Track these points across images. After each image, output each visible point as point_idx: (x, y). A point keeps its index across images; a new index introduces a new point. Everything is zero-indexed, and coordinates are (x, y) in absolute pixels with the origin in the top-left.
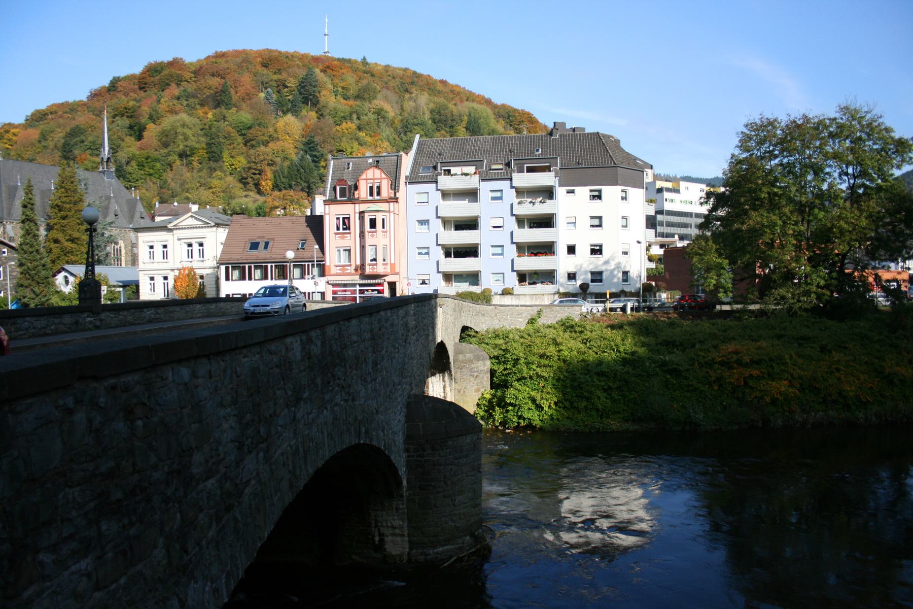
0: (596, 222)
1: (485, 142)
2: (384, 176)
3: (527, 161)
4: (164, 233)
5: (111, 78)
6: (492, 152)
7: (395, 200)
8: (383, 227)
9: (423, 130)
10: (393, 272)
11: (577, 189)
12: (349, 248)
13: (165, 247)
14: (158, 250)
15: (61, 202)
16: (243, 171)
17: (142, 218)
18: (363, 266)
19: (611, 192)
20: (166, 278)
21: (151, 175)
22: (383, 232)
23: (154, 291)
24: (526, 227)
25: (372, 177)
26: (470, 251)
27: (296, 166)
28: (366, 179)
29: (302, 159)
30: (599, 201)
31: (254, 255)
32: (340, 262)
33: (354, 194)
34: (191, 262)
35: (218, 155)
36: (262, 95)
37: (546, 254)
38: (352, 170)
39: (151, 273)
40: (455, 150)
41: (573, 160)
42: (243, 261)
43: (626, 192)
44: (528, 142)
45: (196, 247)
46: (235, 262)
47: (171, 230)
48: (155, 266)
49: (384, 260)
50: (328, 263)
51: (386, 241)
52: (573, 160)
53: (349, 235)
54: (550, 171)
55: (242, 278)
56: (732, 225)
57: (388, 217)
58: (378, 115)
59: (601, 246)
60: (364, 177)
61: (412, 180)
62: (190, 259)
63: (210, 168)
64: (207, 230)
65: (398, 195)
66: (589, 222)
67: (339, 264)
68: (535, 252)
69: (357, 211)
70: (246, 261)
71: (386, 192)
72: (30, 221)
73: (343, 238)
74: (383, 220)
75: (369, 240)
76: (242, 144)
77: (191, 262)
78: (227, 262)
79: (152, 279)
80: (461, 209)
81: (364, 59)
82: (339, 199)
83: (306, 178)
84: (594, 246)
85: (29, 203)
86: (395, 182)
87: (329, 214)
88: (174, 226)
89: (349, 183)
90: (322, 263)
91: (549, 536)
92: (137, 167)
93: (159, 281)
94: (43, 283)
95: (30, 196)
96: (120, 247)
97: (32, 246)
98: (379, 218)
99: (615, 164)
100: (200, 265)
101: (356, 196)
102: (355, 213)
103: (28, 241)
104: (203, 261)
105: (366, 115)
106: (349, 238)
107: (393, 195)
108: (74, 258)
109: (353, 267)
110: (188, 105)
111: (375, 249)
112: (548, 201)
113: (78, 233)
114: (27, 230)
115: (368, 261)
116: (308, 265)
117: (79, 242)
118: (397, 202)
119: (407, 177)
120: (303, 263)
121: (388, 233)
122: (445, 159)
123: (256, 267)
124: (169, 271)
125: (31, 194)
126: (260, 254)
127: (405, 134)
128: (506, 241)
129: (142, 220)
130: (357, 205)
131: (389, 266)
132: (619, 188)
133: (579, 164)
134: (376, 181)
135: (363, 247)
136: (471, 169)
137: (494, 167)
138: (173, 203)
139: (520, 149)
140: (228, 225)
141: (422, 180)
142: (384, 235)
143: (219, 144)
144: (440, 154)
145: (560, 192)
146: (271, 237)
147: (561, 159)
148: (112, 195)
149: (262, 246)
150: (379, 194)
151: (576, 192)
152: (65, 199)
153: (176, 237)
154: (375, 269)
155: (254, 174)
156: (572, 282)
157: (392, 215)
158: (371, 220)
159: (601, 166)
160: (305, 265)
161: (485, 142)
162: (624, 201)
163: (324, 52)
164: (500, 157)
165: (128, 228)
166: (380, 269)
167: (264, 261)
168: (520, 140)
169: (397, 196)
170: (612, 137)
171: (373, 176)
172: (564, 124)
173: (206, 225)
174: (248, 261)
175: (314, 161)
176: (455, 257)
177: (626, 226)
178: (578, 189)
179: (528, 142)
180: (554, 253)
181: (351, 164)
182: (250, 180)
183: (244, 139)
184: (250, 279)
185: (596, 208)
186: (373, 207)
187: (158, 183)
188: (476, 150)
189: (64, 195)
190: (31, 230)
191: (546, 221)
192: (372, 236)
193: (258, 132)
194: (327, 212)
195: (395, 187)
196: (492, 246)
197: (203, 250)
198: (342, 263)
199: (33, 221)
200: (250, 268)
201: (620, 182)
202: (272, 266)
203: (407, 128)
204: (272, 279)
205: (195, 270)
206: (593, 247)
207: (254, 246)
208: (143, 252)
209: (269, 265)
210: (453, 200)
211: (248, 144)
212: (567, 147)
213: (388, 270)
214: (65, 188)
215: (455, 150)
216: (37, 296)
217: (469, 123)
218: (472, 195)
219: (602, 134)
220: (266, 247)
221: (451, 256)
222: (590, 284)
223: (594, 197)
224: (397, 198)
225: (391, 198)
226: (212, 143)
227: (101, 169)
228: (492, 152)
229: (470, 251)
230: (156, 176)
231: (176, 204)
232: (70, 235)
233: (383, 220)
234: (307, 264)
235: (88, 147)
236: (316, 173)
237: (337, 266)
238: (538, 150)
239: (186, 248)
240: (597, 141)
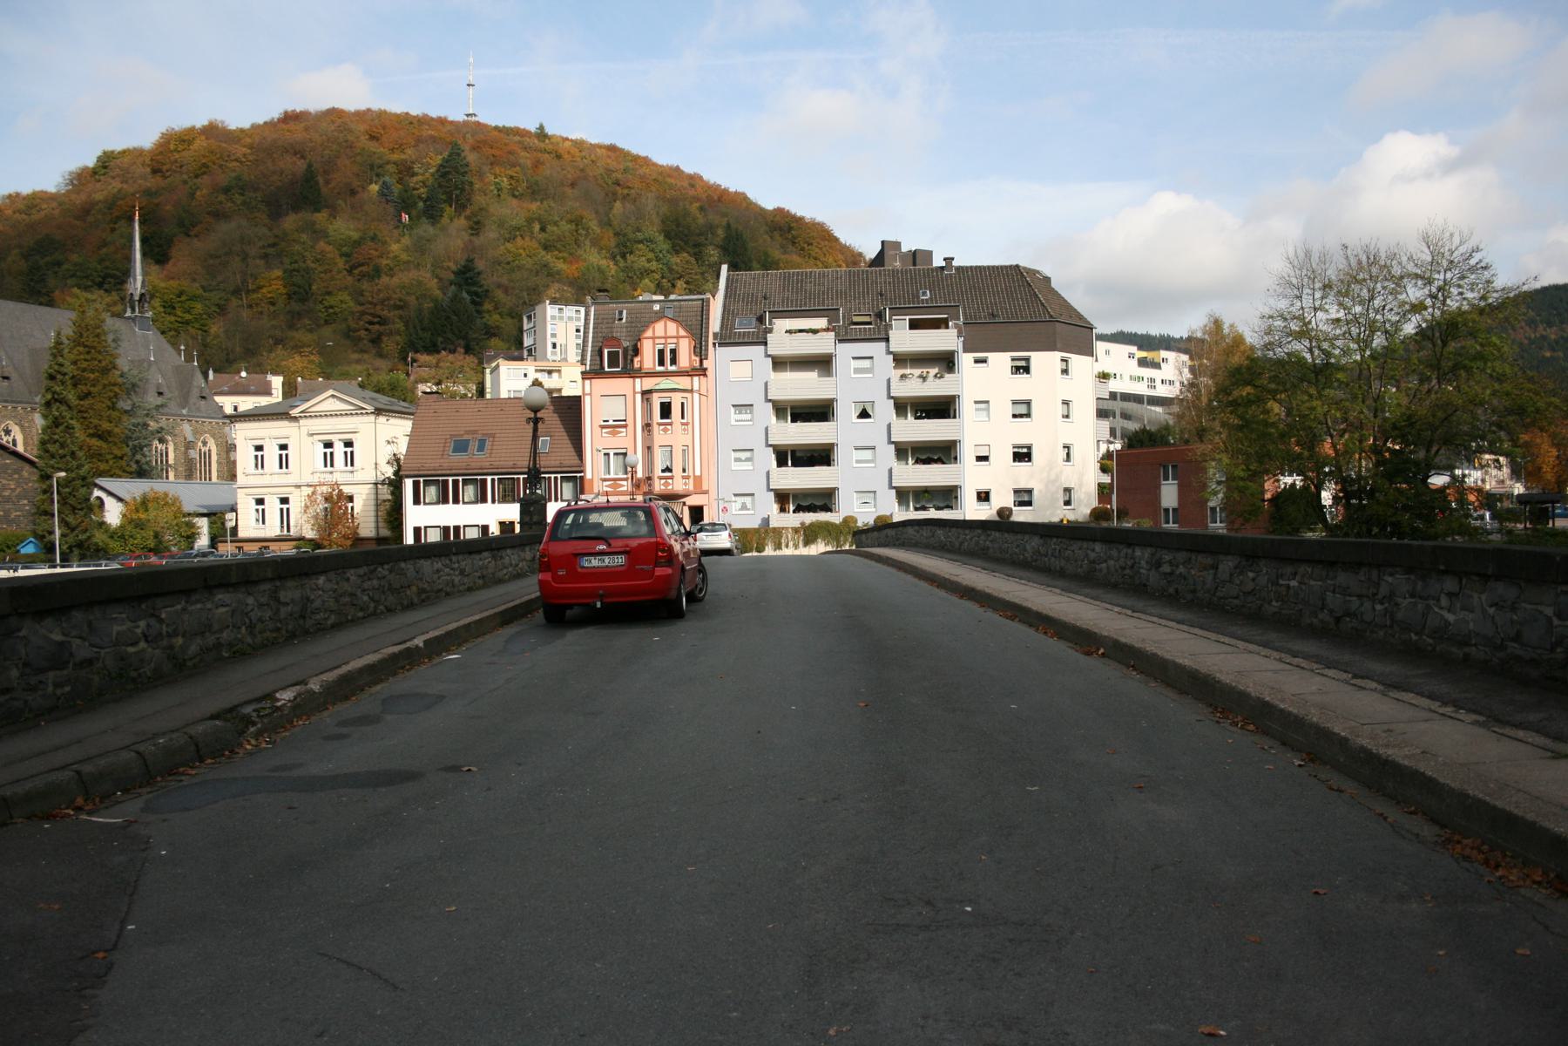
0: (1022, 409)
1: (837, 278)
2: (682, 332)
3: (907, 310)
4: (285, 423)
5: (99, 153)
6: (850, 296)
7: (702, 372)
8: (683, 417)
9: (652, 251)
10: (698, 491)
11: (992, 356)
12: (624, 451)
13: (283, 447)
14: (271, 454)
15: (78, 369)
16: (350, 318)
17: (203, 397)
19: (1045, 362)
20: (284, 501)
21: (187, 323)
22: (683, 424)
23: (264, 523)
24: (909, 415)
26: (820, 456)
27: (444, 311)
28: (654, 338)
29: (455, 298)
30: (1025, 375)
31: (459, 460)
32: (609, 473)
33: (632, 361)
34: (331, 473)
35: (305, 290)
36: (375, 188)
37: (940, 461)
38: (627, 322)
39: (259, 493)
40: (788, 290)
41: (983, 310)
42: (444, 472)
43: (1066, 361)
44: (907, 279)
45: (339, 449)
46: (430, 472)
47: (295, 419)
48: (266, 480)
49: (684, 471)
50: (589, 475)
51: (687, 440)
52: (983, 310)
53: (624, 430)
54: (947, 327)
57: (690, 400)
58: (577, 225)
59: (1029, 448)
60: (649, 333)
61: (728, 339)
62: (349, 468)
63: (289, 312)
64: (360, 418)
65: (706, 363)
66: (1010, 410)
67: (608, 476)
68: (924, 457)
69: (638, 389)
70: (448, 472)
71: (686, 359)
72: (60, 402)
73: (614, 434)
74: (683, 404)
75: (659, 437)
76: (345, 273)
77: (331, 473)
78: (416, 473)
79: (260, 502)
80: (804, 386)
81: (541, 128)
82: (606, 369)
83: (460, 332)
84: (282, 527)
85: (59, 372)
86: (701, 348)
87: (590, 394)
88: (302, 412)
89: (626, 344)
90: (578, 475)
91: (1414, 637)
92: (162, 310)
93: (273, 507)
94: (81, 509)
95: (60, 360)
96: (210, 450)
97: (63, 446)
98: (676, 400)
99: (1051, 316)
100: (348, 478)
101: (637, 365)
102: (635, 393)
103: (56, 437)
104: (352, 472)
105: (556, 224)
106: (624, 434)
107: (697, 364)
108: (103, 466)
110: (244, 203)
111: (668, 454)
112: (947, 375)
113: (108, 424)
114: (56, 418)
115: (658, 472)
116: (556, 478)
117: (110, 439)
118: (705, 375)
119: (715, 335)
120: (516, 476)
121: (690, 426)
122: (774, 304)
123: (465, 482)
124: (293, 489)
125: (62, 356)
126: (474, 459)
127: (624, 256)
128: (880, 440)
129: (203, 402)
130: (638, 381)
131: (691, 480)
132: (1058, 355)
133: (993, 316)
134: (669, 341)
135: (649, 449)
136: (821, 323)
137: (856, 319)
138: (239, 372)
139: (895, 291)
140: (412, 414)
141: (741, 341)
142: (685, 430)
143: (307, 270)
144: (765, 298)
145: (966, 360)
146: (490, 432)
147: (964, 308)
148: (152, 359)
149: (474, 446)
150: (674, 361)
151: (989, 360)
152: (85, 365)
153: (304, 431)
154: (669, 484)
155: (371, 323)
156: (984, 506)
157: (696, 396)
158: (662, 404)
159: (1029, 319)
160: (550, 478)
161: (837, 278)
162: (1065, 376)
163: (467, 115)
164: (864, 304)
165: (179, 416)
166: (678, 485)
167: (480, 471)
168: (893, 276)
169: (705, 366)
170: (1038, 272)
171: (664, 333)
172: (897, 245)
173: (359, 412)
174: (454, 472)
175: (473, 302)
176: (794, 465)
177: (1067, 417)
178: (992, 357)
179: (907, 279)
180: (956, 458)
181: (625, 312)
182: (363, 333)
183: (347, 262)
184: (456, 501)
185: (1022, 387)
187: (200, 338)
188: (823, 292)
189: (82, 357)
190: (63, 418)
191: (942, 408)
192: (665, 430)
193: (372, 252)
194: (587, 390)
195: (700, 351)
196: (857, 448)
197: (262, 456)
198: (612, 476)
199: (66, 403)
200: (456, 483)
201: (1059, 345)
202: (493, 480)
203: (626, 247)
204: (493, 501)
205: (341, 487)
206: (1016, 450)
207: (461, 446)
208: (244, 458)
209: (489, 478)
210: (791, 371)
211: (356, 272)
212: (898, 283)
213: (691, 487)
214: (85, 346)
215: (788, 290)
216: (73, 530)
217: (728, 238)
218: (823, 363)
219: (1025, 268)
220: (481, 448)
221: (786, 465)
222: (1014, 508)
224: (706, 369)
225: (694, 369)
226: (294, 270)
227: (128, 314)
228: (850, 296)
229: (820, 456)
230: (197, 325)
231: (244, 374)
232: (96, 426)
233: (683, 404)
234: (553, 476)
235: (71, 273)
236: (478, 321)
237: (605, 480)
238: (924, 294)
239: (321, 449)
240: (1018, 280)
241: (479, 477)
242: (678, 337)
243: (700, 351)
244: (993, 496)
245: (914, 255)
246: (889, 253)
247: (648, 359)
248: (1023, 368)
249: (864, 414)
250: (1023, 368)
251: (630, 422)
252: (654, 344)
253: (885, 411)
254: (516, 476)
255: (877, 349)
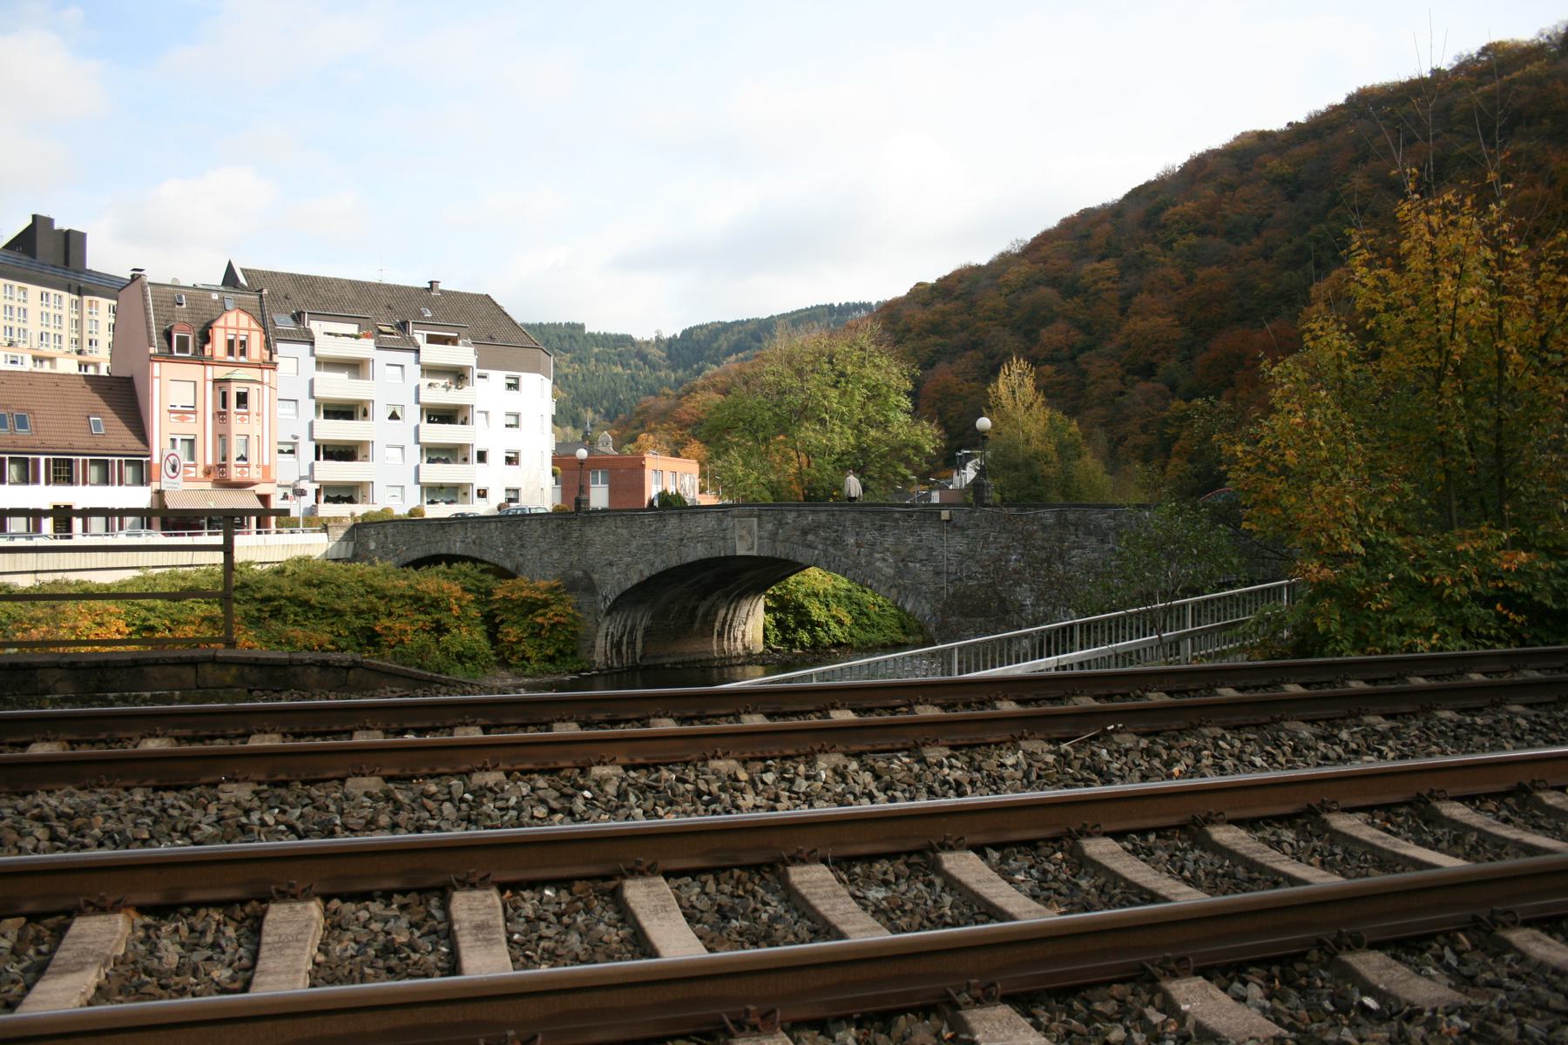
0: (512, 421)
2: (254, 325)
12: (192, 437)
18: (222, 467)
25: (234, 325)
55: (105, 480)
56: (950, 439)
59: (517, 453)
60: (221, 322)
69: (209, 376)
71: (256, 350)
73: (183, 420)
87: (160, 378)
101: (208, 352)
107: (267, 358)
109: (201, 468)
111: (243, 443)
130: (209, 368)
134: (241, 332)
150: (243, 353)
157: (266, 388)
158: (238, 394)
166: (254, 474)
172: (50, 221)
178: (492, 373)
185: (513, 401)
186: (241, 373)
192: (242, 420)
202: (47, 461)
204: (48, 483)
206: (322, 456)
209: (42, 458)
218: (355, 367)
223: (510, 386)
224: (276, 364)
234: (116, 459)
241: (30, 457)
242: (249, 330)
243: (268, 345)
244: (489, 494)
245: (68, 234)
246: (39, 229)
247: (218, 347)
248: (514, 386)
249: (394, 416)
250: (514, 386)
251: (200, 407)
252: (226, 334)
253: (413, 415)
254: (110, 458)
255: (408, 358)
